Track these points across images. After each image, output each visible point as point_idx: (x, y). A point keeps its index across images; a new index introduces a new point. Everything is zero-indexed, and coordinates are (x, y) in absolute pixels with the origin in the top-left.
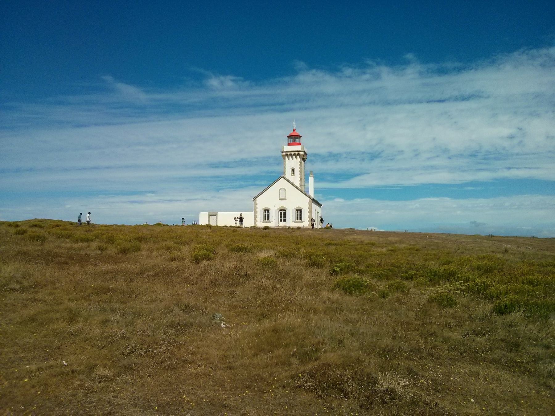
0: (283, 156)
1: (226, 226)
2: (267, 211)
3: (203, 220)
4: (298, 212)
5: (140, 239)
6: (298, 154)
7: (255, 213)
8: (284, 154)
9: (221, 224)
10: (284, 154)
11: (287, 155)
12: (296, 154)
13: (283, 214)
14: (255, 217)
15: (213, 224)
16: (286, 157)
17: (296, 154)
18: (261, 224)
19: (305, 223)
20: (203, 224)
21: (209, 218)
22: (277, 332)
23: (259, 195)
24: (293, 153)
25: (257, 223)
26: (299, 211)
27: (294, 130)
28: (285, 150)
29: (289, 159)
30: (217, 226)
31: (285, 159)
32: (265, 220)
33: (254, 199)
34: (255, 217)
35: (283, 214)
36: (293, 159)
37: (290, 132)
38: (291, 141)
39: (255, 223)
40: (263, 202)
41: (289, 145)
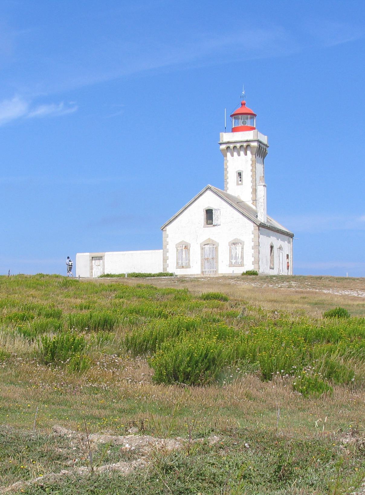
7: (166, 252)
8: (223, 147)
12: (245, 147)
14: (165, 259)
16: (229, 154)
17: (245, 147)
28: (225, 140)
29: (232, 155)
34: (165, 259)
41: (234, 130)
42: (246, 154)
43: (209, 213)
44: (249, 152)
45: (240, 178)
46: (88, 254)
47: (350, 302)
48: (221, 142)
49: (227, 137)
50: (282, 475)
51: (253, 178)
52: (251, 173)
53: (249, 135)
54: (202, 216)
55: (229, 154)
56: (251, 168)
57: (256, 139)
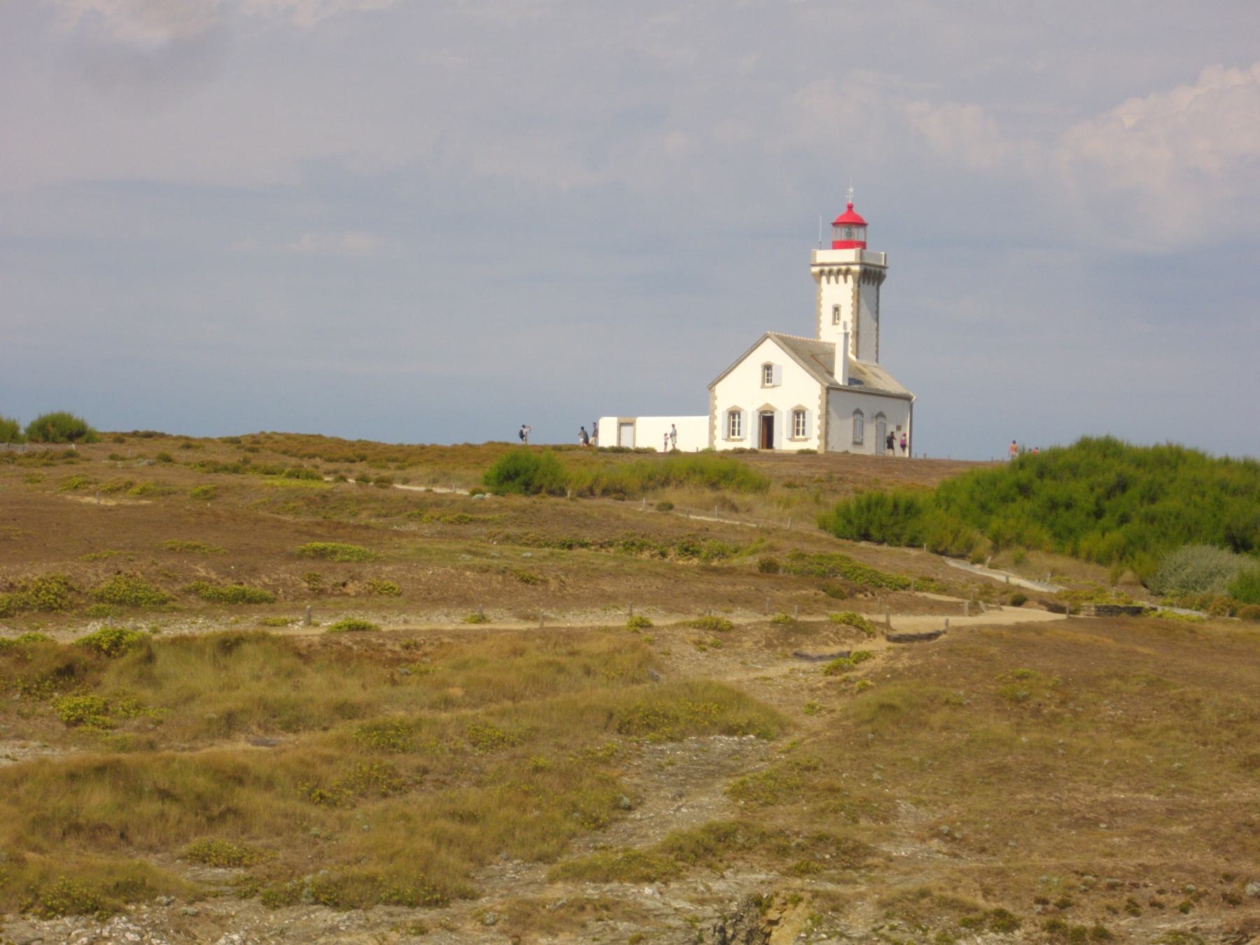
0: (814, 275)
1: (320, 437)
3: (608, 436)
5: (1211, 574)
7: (713, 418)
10: (816, 270)
11: (822, 272)
12: (842, 272)
13: (767, 423)
15: (627, 443)
18: (721, 445)
19: (813, 443)
21: (619, 430)
22: (920, 724)
23: (720, 379)
24: (835, 268)
25: (716, 442)
26: (799, 413)
28: (819, 261)
29: (829, 282)
30: (675, 452)
31: (819, 282)
33: (712, 386)
35: (767, 423)
36: (837, 282)
38: (841, 234)
39: (711, 442)
40: (728, 393)
43: (768, 367)
44: (850, 278)
54: (759, 372)
55: (824, 279)
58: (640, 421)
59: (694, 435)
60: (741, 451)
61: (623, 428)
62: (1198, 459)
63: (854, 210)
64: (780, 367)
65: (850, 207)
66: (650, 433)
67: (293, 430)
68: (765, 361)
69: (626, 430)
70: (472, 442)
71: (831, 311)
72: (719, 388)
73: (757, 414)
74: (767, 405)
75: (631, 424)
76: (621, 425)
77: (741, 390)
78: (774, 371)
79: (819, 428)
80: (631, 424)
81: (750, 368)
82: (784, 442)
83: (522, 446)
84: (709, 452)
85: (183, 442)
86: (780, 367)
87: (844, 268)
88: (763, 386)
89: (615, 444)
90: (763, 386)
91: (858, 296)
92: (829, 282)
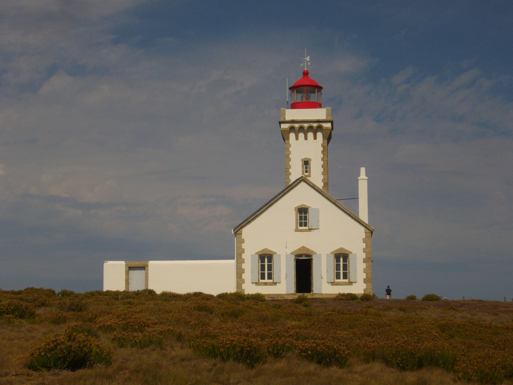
2: (266, 258)
3: (114, 277)
4: (263, 261)
6: (320, 128)
7: (240, 262)
8: (284, 126)
9: (158, 287)
11: (292, 129)
12: (313, 128)
13: (304, 267)
14: (240, 272)
16: (292, 136)
17: (313, 128)
20: (113, 289)
21: (127, 274)
23: (247, 221)
24: (306, 125)
25: (244, 286)
26: (342, 258)
27: (306, 74)
28: (288, 118)
29: (297, 138)
32: (263, 277)
33: (238, 229)
34: (240, 272)
35: (304, 267)
37: (296, 78)
38: (298, 98)
40: (256, 237)
41: (294, 106)
42: (315, 138)
43: (303, 212)
44: (319, 135)
45: (306, 168)
46: (123, 263)
47: (488, 319)
48: (282, 120)
49: (291, 114)
50: (238, 383)
51: (324, 169)
52: (322, 163)
53: (319, 114)
54: (293, 217)
55: (292, 136)
56: (322, 156)
57: (330, 119)
58: (152, 264)
59: (209, 277)
60: (351, 297)
61: (132, 273)
62: (81, 294)
63: (309, 75)
64: (317, 211)
65: (306, 74)
66: (172, 277)
67: (298, 248)
68: (299, 203)
69: (135, 274)
70: (207, 291)
71: (300, 163)
72: (246, 231)
73: (293, 257)
74: (341, 249)
75: (144, 268)
76: (130, 268)
77: (274, 232)
78: (310, 216)
79: (365, 271)
80: (144, 268)
81: (285, 209)
82: (324, 285)
83: (389, 301)
84: (239, 297)
85: (41, 335)
86: (317, 211)
87: (315, 125)
88: (297, 230)
89: (231, 289)
90: (297, 230)
91: (325, 151)
92: (297, 138)
